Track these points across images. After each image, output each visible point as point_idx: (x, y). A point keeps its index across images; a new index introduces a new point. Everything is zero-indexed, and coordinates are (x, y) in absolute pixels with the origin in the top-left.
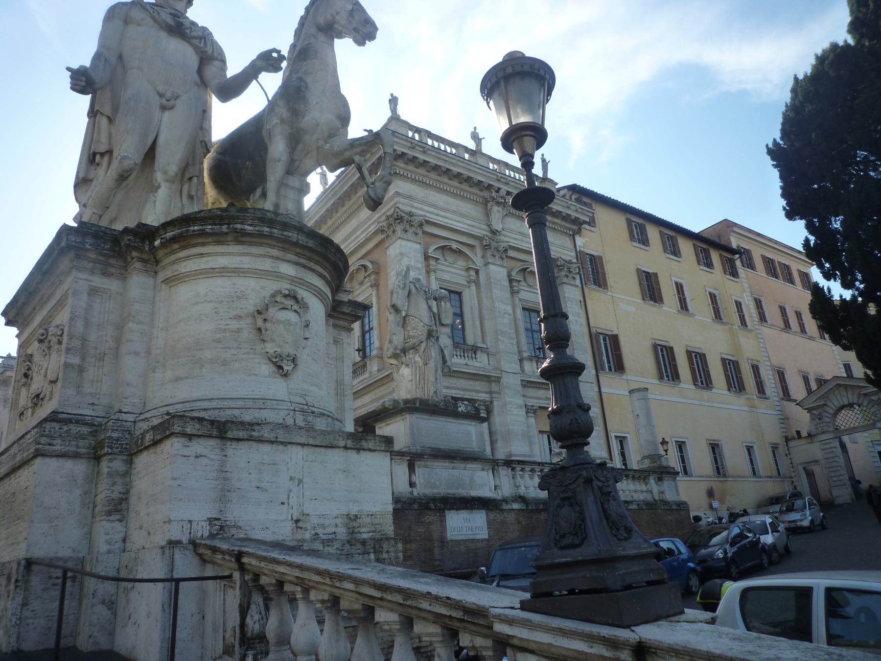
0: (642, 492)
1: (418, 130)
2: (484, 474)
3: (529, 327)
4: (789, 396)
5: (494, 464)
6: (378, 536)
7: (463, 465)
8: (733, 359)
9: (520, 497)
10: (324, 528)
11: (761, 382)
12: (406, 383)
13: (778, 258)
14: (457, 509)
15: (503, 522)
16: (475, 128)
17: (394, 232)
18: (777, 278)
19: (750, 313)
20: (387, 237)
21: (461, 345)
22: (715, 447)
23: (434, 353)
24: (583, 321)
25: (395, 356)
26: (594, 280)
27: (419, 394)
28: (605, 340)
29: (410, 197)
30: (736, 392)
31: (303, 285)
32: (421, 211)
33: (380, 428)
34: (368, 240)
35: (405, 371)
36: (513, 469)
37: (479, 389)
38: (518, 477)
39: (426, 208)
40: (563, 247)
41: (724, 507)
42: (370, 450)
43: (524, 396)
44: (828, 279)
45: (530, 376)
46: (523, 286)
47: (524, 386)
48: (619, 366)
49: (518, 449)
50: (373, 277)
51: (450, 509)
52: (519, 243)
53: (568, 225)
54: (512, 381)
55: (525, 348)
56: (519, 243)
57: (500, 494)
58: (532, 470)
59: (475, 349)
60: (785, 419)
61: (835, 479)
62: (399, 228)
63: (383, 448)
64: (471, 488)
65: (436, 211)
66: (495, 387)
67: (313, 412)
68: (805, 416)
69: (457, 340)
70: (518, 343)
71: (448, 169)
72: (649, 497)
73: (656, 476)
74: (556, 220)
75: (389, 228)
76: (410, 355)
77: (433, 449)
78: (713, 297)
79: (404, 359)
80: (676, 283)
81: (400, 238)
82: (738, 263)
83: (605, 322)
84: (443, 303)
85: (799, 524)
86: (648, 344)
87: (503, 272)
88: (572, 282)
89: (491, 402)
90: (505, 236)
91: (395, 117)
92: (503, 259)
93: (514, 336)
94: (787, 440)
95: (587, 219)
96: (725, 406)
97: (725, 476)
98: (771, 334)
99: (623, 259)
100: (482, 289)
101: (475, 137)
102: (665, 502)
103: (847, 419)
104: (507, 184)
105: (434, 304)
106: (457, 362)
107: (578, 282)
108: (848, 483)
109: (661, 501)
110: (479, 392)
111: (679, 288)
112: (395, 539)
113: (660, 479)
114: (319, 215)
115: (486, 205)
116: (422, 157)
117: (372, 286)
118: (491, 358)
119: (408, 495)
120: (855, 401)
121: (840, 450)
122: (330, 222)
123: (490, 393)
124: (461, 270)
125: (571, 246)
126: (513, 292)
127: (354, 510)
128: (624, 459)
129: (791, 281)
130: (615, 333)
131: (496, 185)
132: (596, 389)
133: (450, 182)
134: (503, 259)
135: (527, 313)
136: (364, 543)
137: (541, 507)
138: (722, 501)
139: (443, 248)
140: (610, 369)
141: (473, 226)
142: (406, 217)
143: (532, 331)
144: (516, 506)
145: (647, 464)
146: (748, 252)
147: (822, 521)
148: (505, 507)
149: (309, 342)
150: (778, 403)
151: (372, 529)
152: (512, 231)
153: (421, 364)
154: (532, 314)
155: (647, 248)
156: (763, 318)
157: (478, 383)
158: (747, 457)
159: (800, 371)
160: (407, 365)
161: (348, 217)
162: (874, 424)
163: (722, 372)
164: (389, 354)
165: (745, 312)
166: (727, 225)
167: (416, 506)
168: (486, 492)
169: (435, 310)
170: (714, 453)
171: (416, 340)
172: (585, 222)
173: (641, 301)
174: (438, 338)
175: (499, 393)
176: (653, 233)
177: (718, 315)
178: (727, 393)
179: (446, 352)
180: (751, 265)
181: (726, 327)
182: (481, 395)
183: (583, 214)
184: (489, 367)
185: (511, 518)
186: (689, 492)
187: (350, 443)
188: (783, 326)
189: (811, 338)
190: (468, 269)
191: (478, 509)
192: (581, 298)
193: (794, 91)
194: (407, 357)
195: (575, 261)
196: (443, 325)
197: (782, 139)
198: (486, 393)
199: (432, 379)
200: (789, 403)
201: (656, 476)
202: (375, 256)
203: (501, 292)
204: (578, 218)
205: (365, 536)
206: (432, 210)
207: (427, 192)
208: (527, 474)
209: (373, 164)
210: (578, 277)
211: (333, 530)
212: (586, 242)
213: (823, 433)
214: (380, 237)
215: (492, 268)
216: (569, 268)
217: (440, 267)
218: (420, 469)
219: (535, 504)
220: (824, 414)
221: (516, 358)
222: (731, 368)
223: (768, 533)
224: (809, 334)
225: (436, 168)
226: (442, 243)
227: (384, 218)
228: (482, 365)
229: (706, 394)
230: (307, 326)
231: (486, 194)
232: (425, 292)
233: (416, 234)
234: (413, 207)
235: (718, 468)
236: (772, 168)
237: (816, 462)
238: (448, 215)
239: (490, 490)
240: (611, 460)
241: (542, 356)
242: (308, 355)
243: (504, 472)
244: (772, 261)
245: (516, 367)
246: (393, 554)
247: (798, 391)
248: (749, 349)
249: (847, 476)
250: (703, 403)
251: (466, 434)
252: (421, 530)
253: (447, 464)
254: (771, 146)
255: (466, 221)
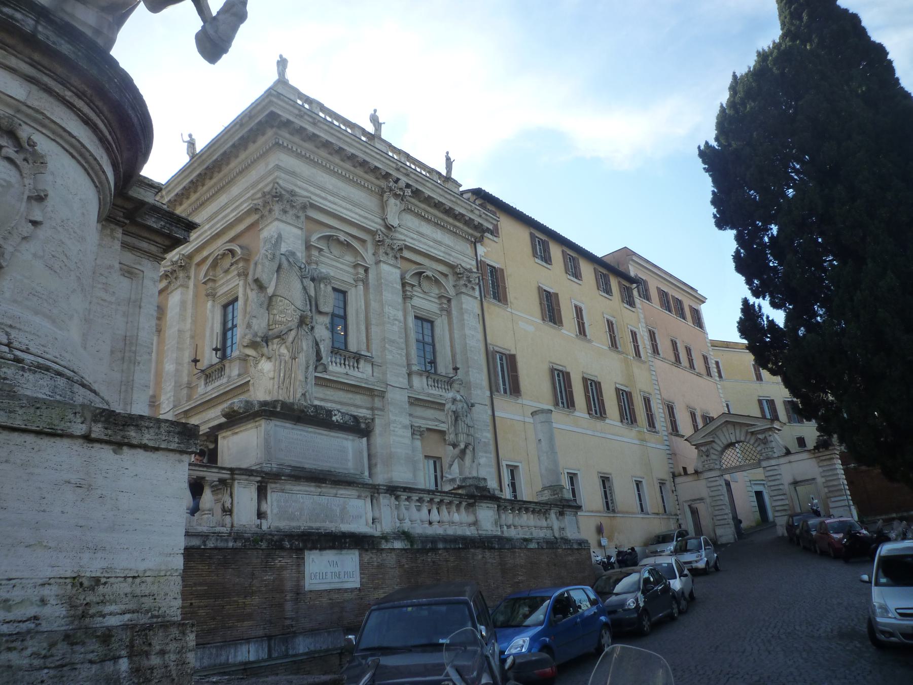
0: (541, 528)
1: (308, 100)
2: (360, 503)
3: (421, 338)
4: (677, 431)
5: (374, 491)
6: (144, 620)
7: (333, 491)
8: (627, 389)
9: (404, 533)
10: (9, 609)
11: (652, 415)
12: (266, 380)
13: (672, 292)
14: (321, 549)
15: (380, 566)
16: (375, 111)
17: (270, 211)
18: (670, 311)
19: (644, 344)
20: (262, 217)
21: (341, 350)
22: (605, 480)
23: (306, 345)
24: (480, 336)
25: (253, 345)
26: (494, 293)
27: (282, 396)
28: (501, 359)
29: (293, 174)
30: (628, 423)
31: (44, 126)
32: (304, 192)
33: (224, 438)
34: (239, 220)
35: (266, 366)
36: (397, 498)
37: (358, 402)
38: (403, 508)
39: (312, 189)
40: (464, 255)
41: (613, 545)
42: (145, 447)
43: (410, 415)
44: (758, 297)
45: (419, 393)
46: (417, 291)
47: (411, 404)
48: (515, 389)
49: (401, 475)
50: (241, 264)
51: (311, 549)
52: (416, 243)
53: (470, 231)
54: (398, 397)
55: (414, 360)
56: (416, 243)
57: (379, 529)
58: (420, 500)
59: (358, 357)
60: (673, 455)
61: (719, 518)
62: (277, 208)
63: (173, 446)
64: (342, 520)
65: (323, 194)
66: (378, 403)
67: (18, 360)
68: (694, 452)
69: (337, 345)
70: (408, 355)
71: (340, 148)
72: (548, 534)
73: (556, 510)
74: (458, 224)
75: (264, 206)
76: (274, 345)
77: (295, 468)
78: (610, 324)
79: (265, 350)
80: (576, 307)
81: (277, 219)
82: (635, 293)
83: (503, 340)
84: (322, 286)
85: (694, 565)
86: (545, 368)
87: (396, 273)
88: (471, 293)
89: (373, 420)
90: (401, 234)
91: (282, 81)
92: (397, 258)
93: (403, 346)
94: (674, 476)
95: (491, 227)
96: (619, 438)
97: (614, 511)
98: (662, 367)
99: (526, 276)
100: (371, 290)
101: (374, 119)
102: (566, 541)
103: (731, 457)
104: (407, 175)
105: (311, 286)
106: (336, 370)
107: (477, 294)
108: (731, 522)
109: (562, 538)
110: (358, 406)
111: (579, 311)
112: (181, 625)
113: (561, 514)
114: (181, 187)
115: (382, 196)
116: (311, 129)
117: (239, 275)
118: (376, 369)
119: (254, 529)
120: (742, 439)
121: (725, 489)
122: (193, 197)
123: (372, 409)
124: (348, 266)
125: (473, 255)
126: (406, 298)
127: (93, 566)
128: (514, 491)
129: (683, 316)
130: (513, 352)
131: (395, 174)
132: (490, 412)
133: (342, 163)
134: (397, 258)
135: (420, 322)
136: (106, 637)
137: (429, 546)
138: (610, 539)
139: (328, 238)
140: (505, 392)
141: (366, 218)
142: (287, 196)
143: (424, 343)
144: (398, 545)
145: (546, 496)
146: (645, 282)
147: (716, 563)
148: (384, 545)
149: (41, 233)
150: (666, 438)
151: (131, 606)
152: (409, 229)
153: (287, 358)
154: (425, 324)
155: (549, 266)
156: (655, 350)
157: (358, 397)
158: (636, 493)
159: (688, 407)
160: (269, 358)
161: (217, 192)
162: (760, 461)
163: (616, 402)
164: (246, 341)
165: (639, 343)
166: (626, 253)
167: (264, 545)
168: (361, 527)
169: (312, 293)
170: (604, 487)
171: (282, 327)
172: (488, 230)
173: (540, 321)
174: (312, 328)
175: (382, 410)
176: (556, 251)
177: (614, 344)
178: (620, 424)
179: (322, 347)
180: (647, 297)
181: (621, 356)
182: (361, 410)
183: (487, 220)
184: (372, 379)
185: (391, 560)
186: (581, 527)
187: (98, 430)
188: (673, 359)
189: (699, 375)
190: (356, 266)
191: (349, 548)
192: (480, 313)
193: (733, 89)
194: (270, 347)
195: (475, 270)
196: (320, 313)
197: (717, 139)
198: (368, 409)
199: (301, 377)
200: (677, 438)
201: (556, 510)
202: (244, 241)
203: (392, 295)
204: (482, 225)
205: (113, 621)
206: (318, 192)
207: (314, 171)
208: (413, 505)
209: (251, 130)
210: (477, 288)
211: (31, 611)
212: (488, 252)
213: (711, 470)
214: (254, 217)
215: (384, 267)
216: (468, 277)
217: (322, 259)
218: (275, 495)
219: (422, 542)
220: (712, 451)
221: (404, 371)
222: (625, 398)
223: (675, 578)
224: (697, 370)
225: (326, 145)
226: (328, 233)
227: (259, 195)
228: (365, 376)
229: (599, 424)
230: (40, 198)
231: (383, 183)
232: (300, 268)
233: (298, 217)
234: (296, 185)
235: (607, 503)
236: (703, 171)
237: (701, 499)
238: (337, 200)
239: (367, 524)
240: (501, 491)
241: (433, 371)
242: (35, 255)
243: (385, 500)
244: (666, 294)
245: (404, 382)
246: (173, 657)
247: (685, 427)
248: (642, 381)
249: (731, 515)
250: (596, 434)
251: (338, 451)
252: (269, 577)
253: (312, 489)
254: (702, 148)
255: (358, 210)
